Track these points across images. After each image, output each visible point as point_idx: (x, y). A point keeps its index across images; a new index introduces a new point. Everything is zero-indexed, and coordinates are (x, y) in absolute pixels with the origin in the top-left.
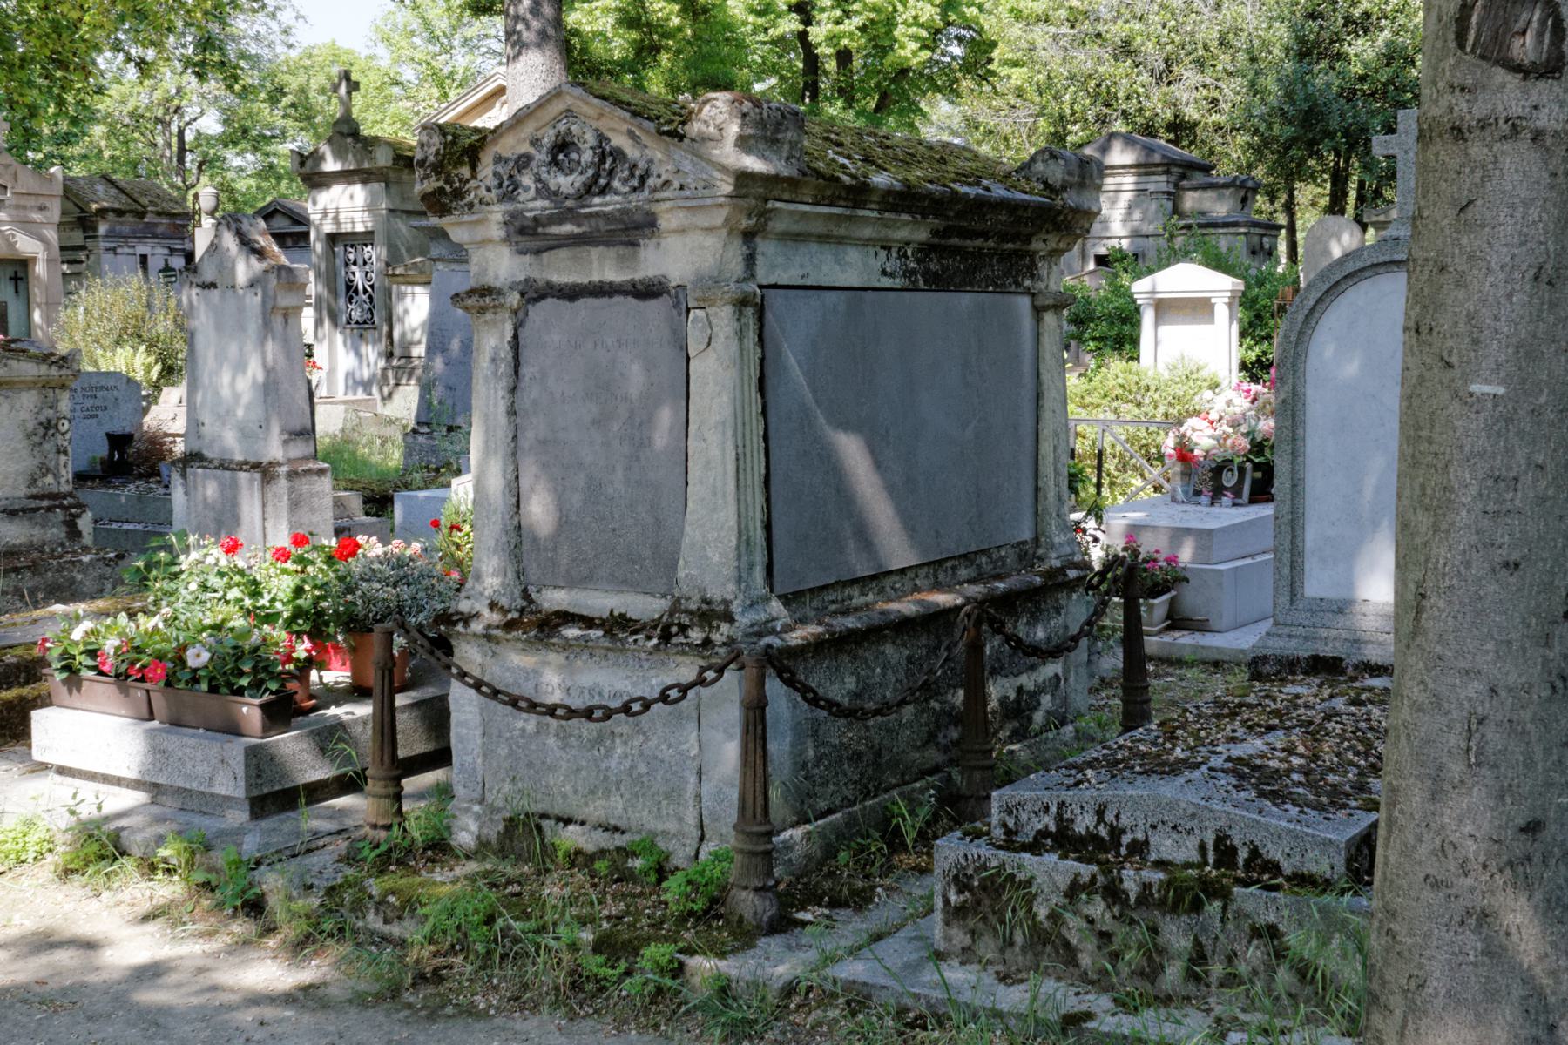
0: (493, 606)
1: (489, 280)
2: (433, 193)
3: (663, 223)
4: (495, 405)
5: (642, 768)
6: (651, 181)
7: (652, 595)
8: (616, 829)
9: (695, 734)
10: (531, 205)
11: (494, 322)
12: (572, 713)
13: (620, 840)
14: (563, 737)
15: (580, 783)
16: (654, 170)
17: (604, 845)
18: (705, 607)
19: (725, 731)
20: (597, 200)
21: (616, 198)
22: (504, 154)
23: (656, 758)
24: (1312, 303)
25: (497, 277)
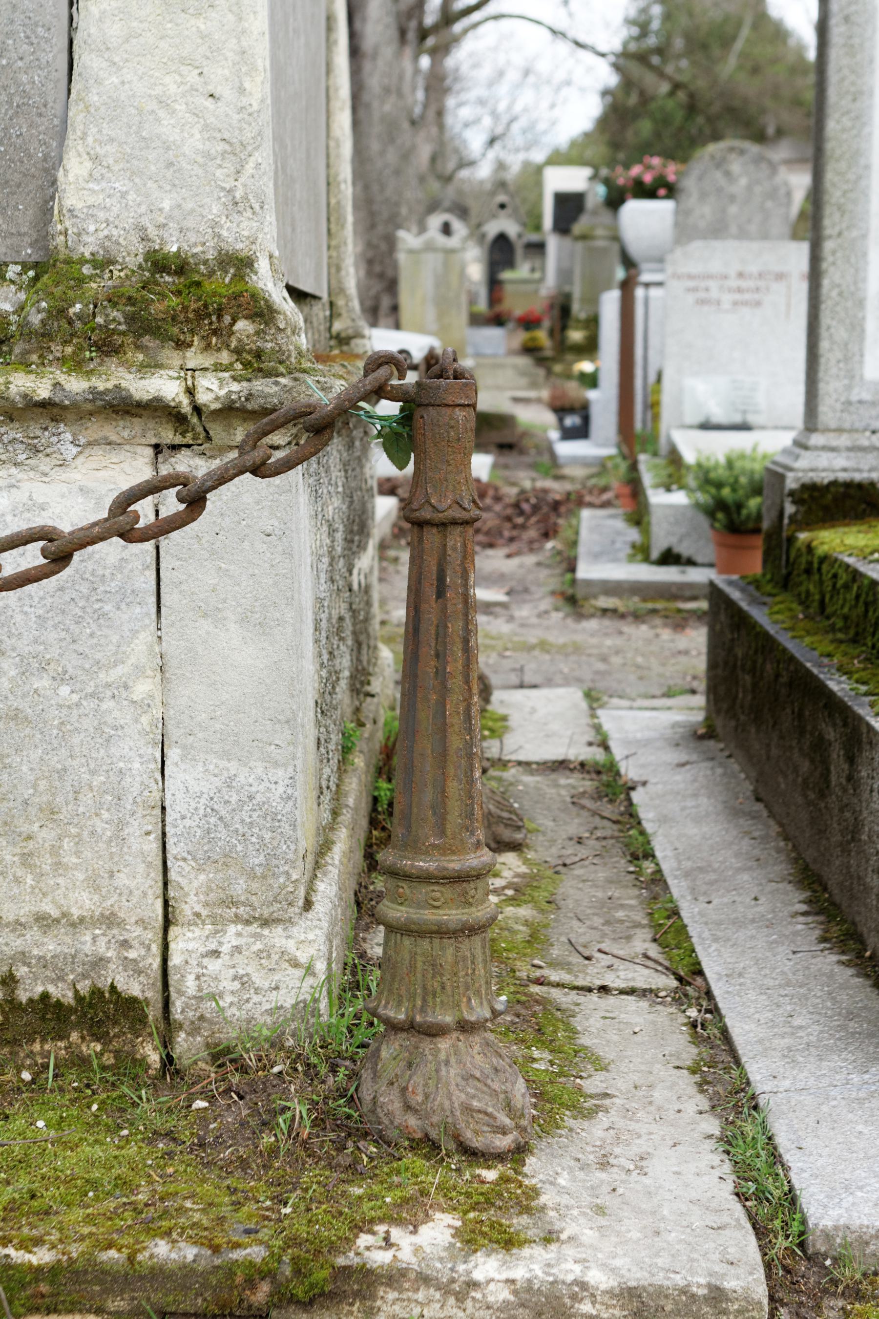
9: (147, 636)
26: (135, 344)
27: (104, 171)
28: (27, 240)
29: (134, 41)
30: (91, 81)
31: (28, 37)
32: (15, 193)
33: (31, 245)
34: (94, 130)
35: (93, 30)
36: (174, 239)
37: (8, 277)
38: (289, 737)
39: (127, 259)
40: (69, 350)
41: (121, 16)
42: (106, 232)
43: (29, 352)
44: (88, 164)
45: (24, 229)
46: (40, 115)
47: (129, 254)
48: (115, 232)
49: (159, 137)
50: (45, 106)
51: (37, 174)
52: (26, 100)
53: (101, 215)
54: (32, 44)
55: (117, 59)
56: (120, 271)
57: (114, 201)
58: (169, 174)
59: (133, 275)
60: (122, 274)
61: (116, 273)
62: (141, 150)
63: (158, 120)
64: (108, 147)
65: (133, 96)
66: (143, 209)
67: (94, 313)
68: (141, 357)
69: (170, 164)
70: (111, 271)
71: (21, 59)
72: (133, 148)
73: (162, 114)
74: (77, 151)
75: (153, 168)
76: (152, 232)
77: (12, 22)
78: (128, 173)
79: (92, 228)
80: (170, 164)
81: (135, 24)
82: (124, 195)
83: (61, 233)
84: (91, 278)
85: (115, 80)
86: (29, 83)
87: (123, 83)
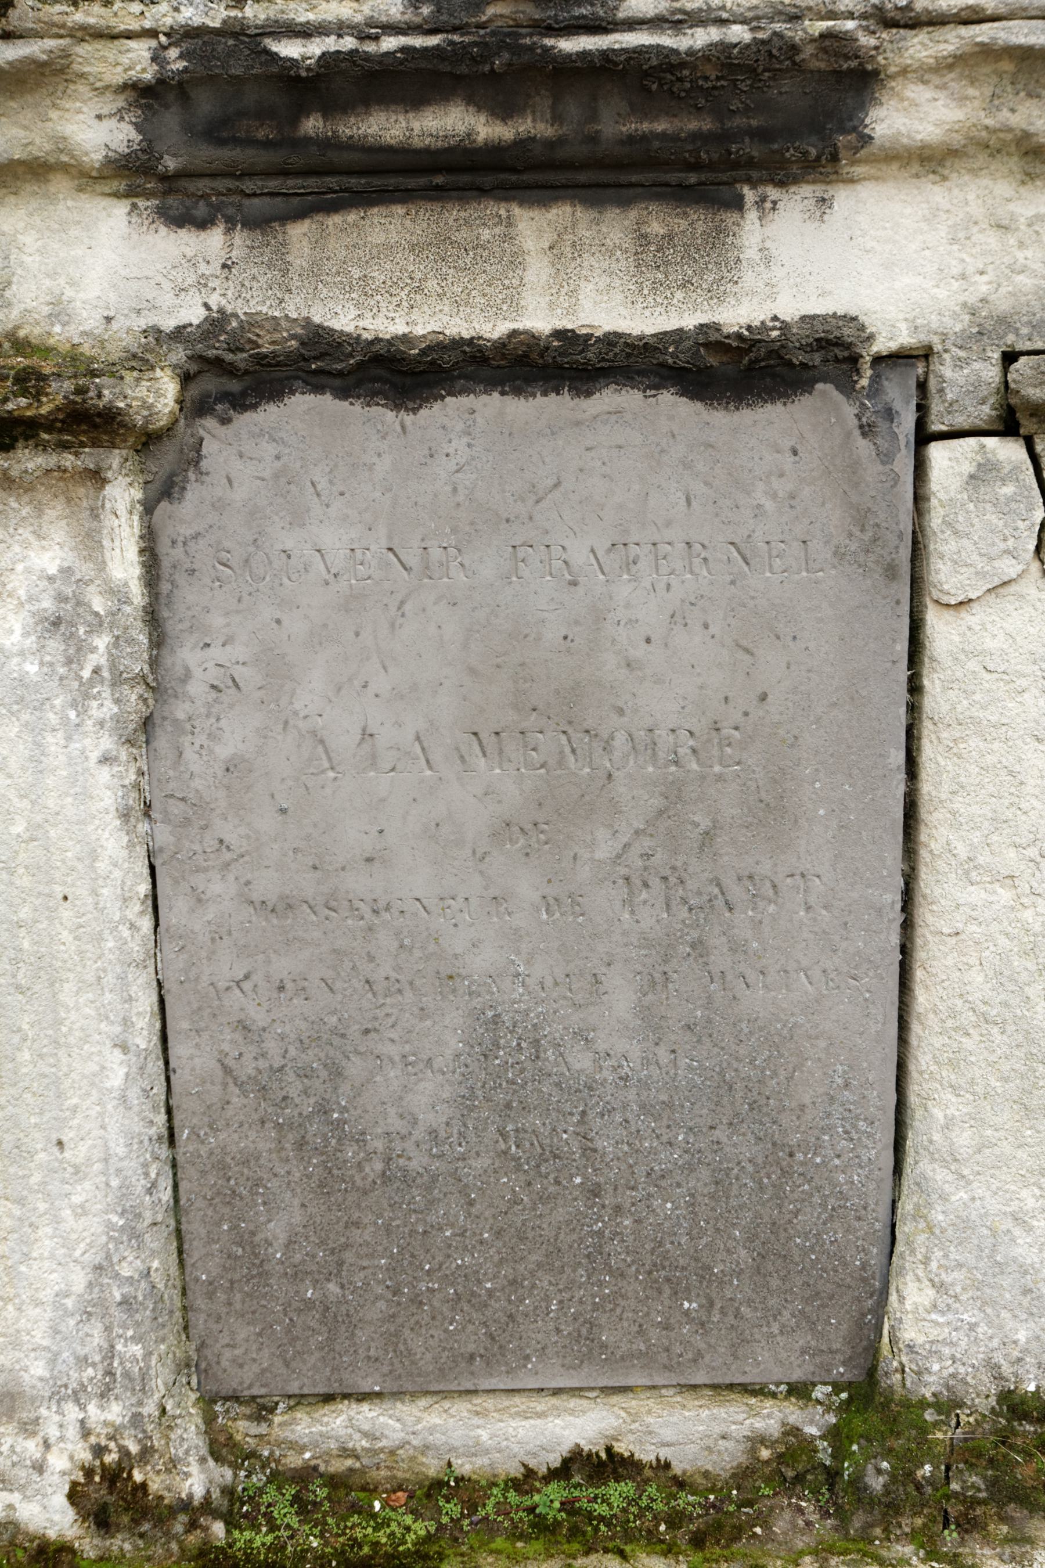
25: (59, 310)
26: (998, 1514)
27: (951, 1301)
28: (839, 1357)
29: (987, 1151)
30: (935, 1197)
31: (846, 1132)
32: (827, 1306)
33: (844, 1364)
34: (939, 1254)
35: (936, 1137)
36: (1031, 1376)
37: (813, 1396)
38: (210, 700)
39: (977, 1401)
40: (919, 1521)
41: (972, 1122)
42: (951, 1370)
43: (872, 1526)
44: (931, 1292)
45: (835, 1346)
46: (859, 1219)
47: (978, 1395)
48: (962, 1370)
49: (1015, 1260)
50: (865, 1208)
51: (853, 1284)
52: (842, 1202)
53: (947, 1351)
54: (852, 1140)
55: (966, 1172)
56: (968, 1415)
57: (961, 1334)
58: (1026, 1301)
59: (984, 1421)
60: (971, 1419)
61: (963, 1417)
62: (994, 1276)
63: (1013, 1240)
64: (956, 1274)
65: (986, 1214)
66: (995, 1343)
67: (947, 1478)
68: (1005, 1529)
69: (1027, 1291)
70: (957, 1415)
71: (838, 1156)
72: (985, 1274)
73: (1017, 1232)
74: (916, 1275)
75: (1008, 1296)
76: (1007, 1370)
77: (829, 1115)
78: (979, 1303)
79: (936, 1367)
80: (1027, 1291)
81: (989, 1132)
82: (973, 1327)
83: (896, 1370)
84: (936, 1424)
85: (963, 1195)
86: (846, 1183)
87: (973, 1199)
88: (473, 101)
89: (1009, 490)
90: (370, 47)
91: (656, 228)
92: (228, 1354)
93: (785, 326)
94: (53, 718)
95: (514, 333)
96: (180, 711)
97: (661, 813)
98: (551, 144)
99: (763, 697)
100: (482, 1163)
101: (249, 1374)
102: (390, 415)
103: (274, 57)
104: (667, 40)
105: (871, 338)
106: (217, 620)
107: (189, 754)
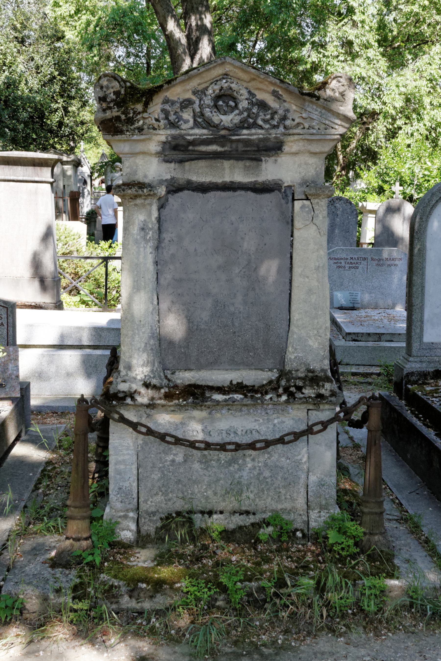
0: (147, 385)
1: (140, 177)
2: (110, 120)
3: (286, 148)
4: (145, 257)
5: (267, 474)
6: (288, 123)
7: (262, 370)
8: (247, 513)
10: (192, 132)
11: (144, 205)
12: (208, 446)
13: (252, 519)
14: (205, 462)
15: (219, 488)
16: (290, 116)
17: (242, 523)
18: (310, 374)
19: (326, 445)
20: (245, 132)
21: (260, 131)
22: (171, 98)
23: (277, 466)
24: (434, 202)
25: (145, 176)
88: (218, 145)
89: (307, 209)
90: (201, 137)
91: (248, 164)
92: (167, 362)
93: (269, 181)
94: (142, 246)
95: (223, 181)
96: (163, 245)
97: (247, 265)
98: (230, 151)
99: (265, 244)
100: (215, 327)
101: (171, 365)
102: (201, 194)
103: (186, 139)
104: (249, 137)
105: (284, 183)
106: (170, 230)
107: (165, 253)
